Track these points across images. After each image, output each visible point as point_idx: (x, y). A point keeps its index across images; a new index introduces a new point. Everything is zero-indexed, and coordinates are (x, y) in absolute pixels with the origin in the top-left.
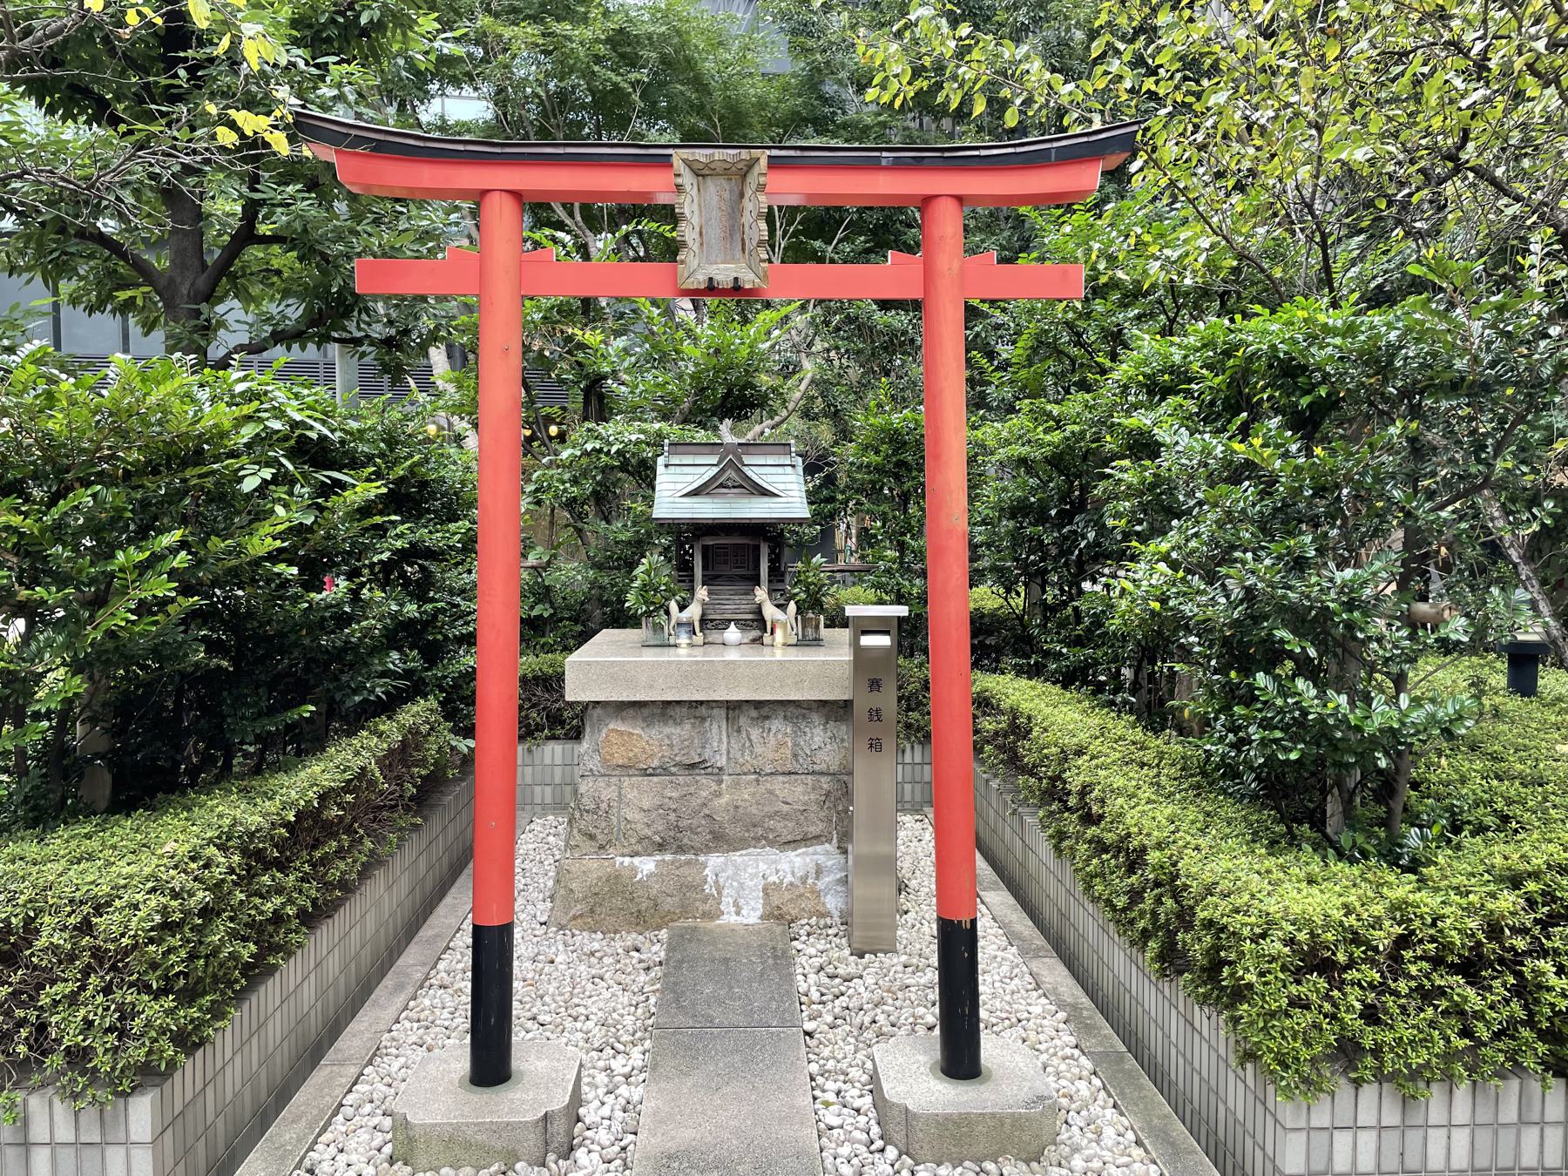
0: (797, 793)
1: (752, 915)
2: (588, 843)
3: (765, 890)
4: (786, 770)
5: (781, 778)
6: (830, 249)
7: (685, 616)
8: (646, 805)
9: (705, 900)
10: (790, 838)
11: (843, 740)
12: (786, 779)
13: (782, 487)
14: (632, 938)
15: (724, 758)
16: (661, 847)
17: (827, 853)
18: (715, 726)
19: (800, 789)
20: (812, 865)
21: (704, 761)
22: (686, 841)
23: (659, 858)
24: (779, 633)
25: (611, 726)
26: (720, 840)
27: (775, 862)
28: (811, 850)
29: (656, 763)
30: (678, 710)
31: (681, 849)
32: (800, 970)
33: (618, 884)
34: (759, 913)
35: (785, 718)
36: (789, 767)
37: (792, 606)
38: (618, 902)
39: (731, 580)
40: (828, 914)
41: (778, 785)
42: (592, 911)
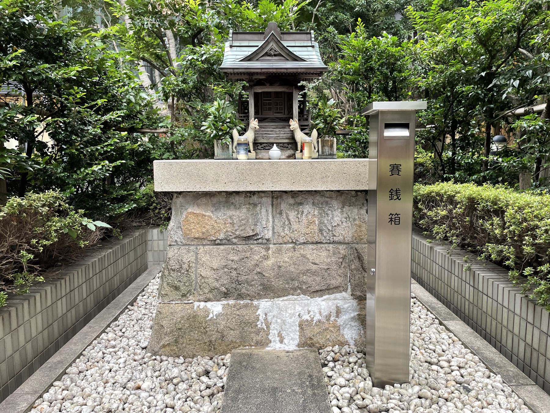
0: (321, 256)
1: (291, 343)
2: (174, 292)
3: (300, 325)
4: (314, 240)
5: (311, 246)
6: (315, 10)
7: (243, 138)
8: (215, 265)
9: (258, 332)
10: (317, 288)
11: (354, 220)
12: (314, 246)
13: (307, 57)
14: (205, 362)
15: (271, 233)
16: (226, 295)
17: (344, 299)
18: (264, 210)
19: (324, 254)
20: (334, 307)
21: (256, 235)
22: (243, 291)
23: (225, 302)
24: (306, 150)
25: (190, 210)
26: (268, 290)
27: (307, 305)
28: (332, 296)
29: (222, 236)
30: (237, 198)
31: (240, 296)
32: (334, 402)
33: (195, 322)
34: (297, 342)
35: (313, 204)
36: (317, 239)
37: (315, 133)
38: (195, 335)
39: (273, 120)
40: (347, 343)
41: (309, 251)
42: (176, 341)
